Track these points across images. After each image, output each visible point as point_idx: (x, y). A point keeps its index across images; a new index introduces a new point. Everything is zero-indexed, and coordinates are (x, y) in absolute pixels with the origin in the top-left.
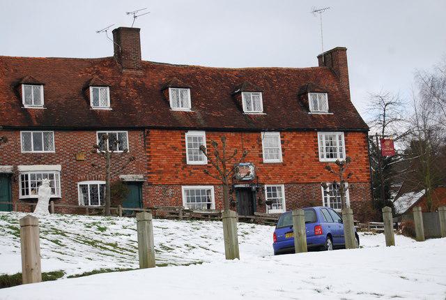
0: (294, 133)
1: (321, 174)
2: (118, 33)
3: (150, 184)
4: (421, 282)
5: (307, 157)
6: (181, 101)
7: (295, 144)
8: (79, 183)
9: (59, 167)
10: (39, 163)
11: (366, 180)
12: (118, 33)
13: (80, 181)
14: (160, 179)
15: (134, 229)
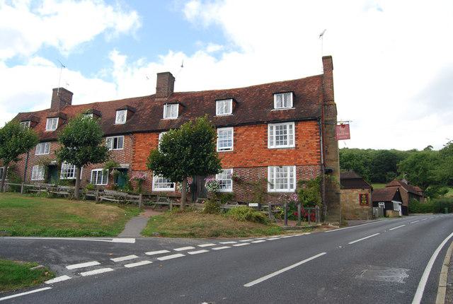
11: (315, 162)
13: (93, 169)
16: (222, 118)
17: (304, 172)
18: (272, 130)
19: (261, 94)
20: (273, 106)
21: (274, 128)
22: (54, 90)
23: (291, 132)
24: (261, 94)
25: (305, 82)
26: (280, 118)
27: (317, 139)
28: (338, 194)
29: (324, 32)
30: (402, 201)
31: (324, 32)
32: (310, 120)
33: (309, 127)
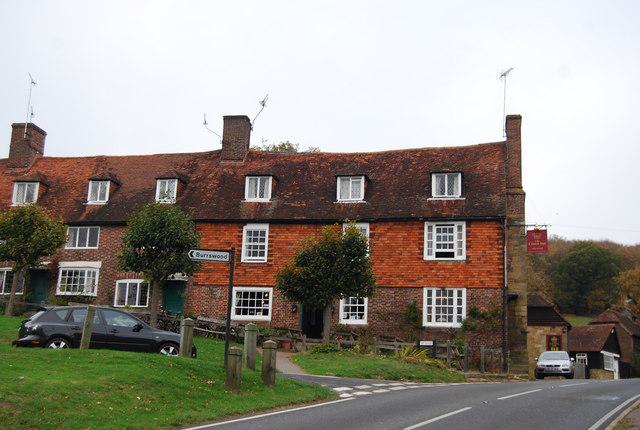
0: (391, 224)
1: (426, 276)
2: (229, 120)
3: (196, 284)
4: (31, 426)
5: (405, 255)
6: (257, 193)
7: (390, 238)
8: (118, 282)
9: (98, 264)
10: (80, 259)
11: (495, 285)
12: (229, 120)
13: (119, 279)
14: (207, 279)
15: (106, 341)
16: (348, 207)
17: (478, 298)
18: (431, 236)
19: (406, 168)
20: (430, 191)
21: (435, 229)
22: (16, 127)
23: (460, 236)
24: (406, 168)
25: (477, 154)
26: (443, 215)
27: (499, 249)
28: (525, 333)
29: (508, 72)
30: (619, 353)
31: (508, 72)
32: (490, 220)
33: (486, 231)
